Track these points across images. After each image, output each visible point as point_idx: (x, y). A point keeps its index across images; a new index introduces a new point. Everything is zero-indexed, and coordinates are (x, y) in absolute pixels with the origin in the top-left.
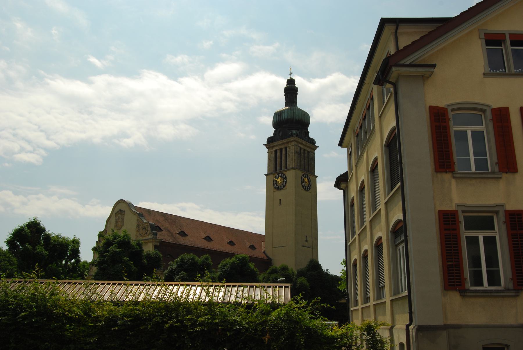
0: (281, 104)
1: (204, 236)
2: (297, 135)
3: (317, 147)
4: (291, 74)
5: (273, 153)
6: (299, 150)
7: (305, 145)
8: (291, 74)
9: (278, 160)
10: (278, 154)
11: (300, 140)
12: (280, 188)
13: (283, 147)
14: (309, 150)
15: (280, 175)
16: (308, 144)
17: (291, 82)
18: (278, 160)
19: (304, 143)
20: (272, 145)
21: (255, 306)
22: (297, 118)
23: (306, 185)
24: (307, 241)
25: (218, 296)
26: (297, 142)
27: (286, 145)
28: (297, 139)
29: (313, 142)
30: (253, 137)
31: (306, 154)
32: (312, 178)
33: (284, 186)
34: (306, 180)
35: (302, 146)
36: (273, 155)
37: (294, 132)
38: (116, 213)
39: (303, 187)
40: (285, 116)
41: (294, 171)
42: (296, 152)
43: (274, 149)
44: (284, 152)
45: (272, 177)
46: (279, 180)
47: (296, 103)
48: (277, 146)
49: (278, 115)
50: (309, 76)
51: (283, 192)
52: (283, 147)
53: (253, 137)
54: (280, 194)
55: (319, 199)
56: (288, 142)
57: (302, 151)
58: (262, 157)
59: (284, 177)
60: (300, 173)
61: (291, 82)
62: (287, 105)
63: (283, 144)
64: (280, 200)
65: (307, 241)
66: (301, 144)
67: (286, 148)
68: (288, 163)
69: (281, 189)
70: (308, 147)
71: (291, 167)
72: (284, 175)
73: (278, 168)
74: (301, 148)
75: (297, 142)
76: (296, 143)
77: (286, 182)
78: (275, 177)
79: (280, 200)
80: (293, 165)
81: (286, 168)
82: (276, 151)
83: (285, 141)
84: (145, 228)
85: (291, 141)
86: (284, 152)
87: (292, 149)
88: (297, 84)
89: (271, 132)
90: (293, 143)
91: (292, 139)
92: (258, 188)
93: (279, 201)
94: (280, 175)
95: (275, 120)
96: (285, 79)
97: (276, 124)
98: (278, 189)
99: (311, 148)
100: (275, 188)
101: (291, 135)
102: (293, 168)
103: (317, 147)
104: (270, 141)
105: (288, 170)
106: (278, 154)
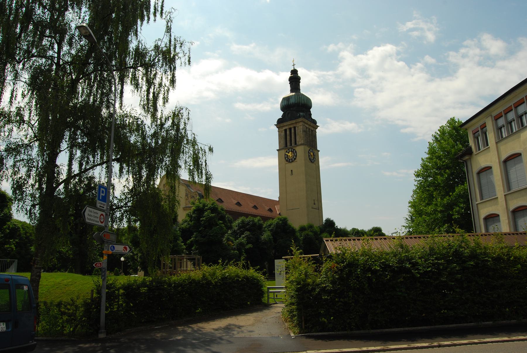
0: (287, 92)
1: (236, 202)
2: (304, 117)
3: (318, 126)
4: (294, 65)
5: (283, 131)
6: (305, 129)
7: (310, 125)
8: (294, 65)
9: (288, 137)
10: (288, 132)
11: (306, 121)
12: (291, 161)
13: (292, 126)
14: (313, 129)
15: (290, 150)
16: (312, 124)
17: (294, 72)
18: (288, 137)
19: (309, 123)
20: (282, 125)
21: (304, 272)
22: (303, 102)
23: (312, 158)
24: (314, 204)
25: (38, 166)
26: (304, 122)
27: (294, 125)
28: (304, 119)
29: (314, 122)
30: (228, 120)
31: (311, 133)
32: (315, 152)
33: (295, 159)
34: (312, 154)
35: (307, 126)
36: (283, 134)
37: (301, 114)
38: (164, 185)
39: (310, 159)
40: (292, 101)
41: (303, 146)
42: (304, 131)
43: (284, 128)
44: (293, 131)
45: (283, 152)
46: (290, 154)
47: (300, 90)
48: (286, 126)
49: (286, 99)
50: (309, 68)
51: (293, 164)
52: (292, 126)
53: (228, 120)
54: (290, 166)
55: (321, 168)
56: (296, 123)
57: (308, 130)
58: (274, 134)
59: (294, 152)
60: (308, 149)
61: (294, 72)
62: (292, 91)
63: (292, 124)
64: (292, 171)
65: (314, 204)
66: (307, 124)
67: (295, 128)
68: (297, 140)
69: (292, 161)
70: (312, 126)
71: (300, 143)
72: (294, 150)
73: (288, 144)
74: (307, 128)
75: (304, 122)
76: (303, 123)
77: (296, 156)
78: (286, 152)
79: (292, 171)
80: (302, 142)
81: (296, 144)
82: (286, 130)
83: (294, 122)
84: (193, 197)
85: (299, 122)
86: (293, 131)
87: (300, 128)
88: (299, 74)
89: (280, 114)
90: (301, 124)
91: (300, 120)
92: (271, 162)
93: (290, 171)
94: (290, 150)
95: (284, 104)
96: (287, 72)
97: (283, 108)
98: (289, 162)
99: (314, 127)
100: (287, 161)
101: (300, 117)
102: (301, 144)
103: (318, 126)
104: (280, 122)
105: (298, 146)
106: (288, 132)
